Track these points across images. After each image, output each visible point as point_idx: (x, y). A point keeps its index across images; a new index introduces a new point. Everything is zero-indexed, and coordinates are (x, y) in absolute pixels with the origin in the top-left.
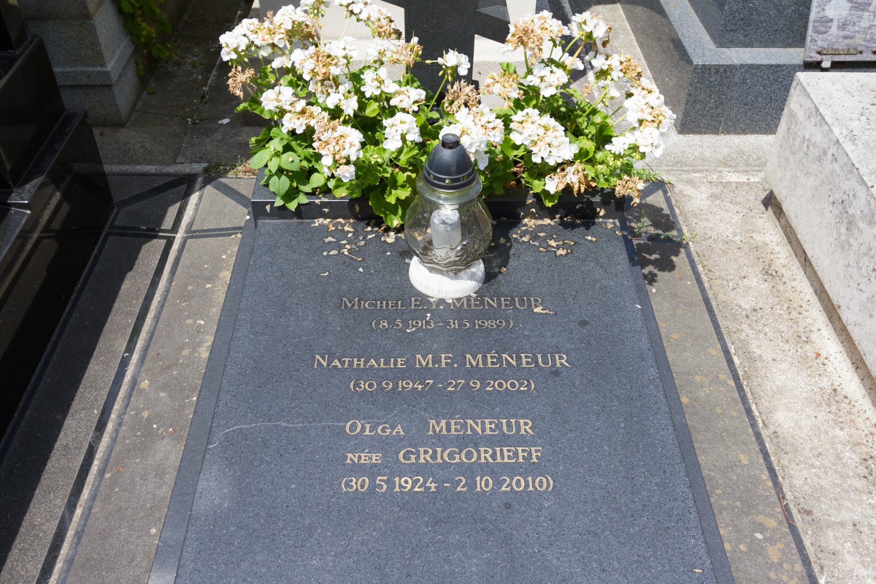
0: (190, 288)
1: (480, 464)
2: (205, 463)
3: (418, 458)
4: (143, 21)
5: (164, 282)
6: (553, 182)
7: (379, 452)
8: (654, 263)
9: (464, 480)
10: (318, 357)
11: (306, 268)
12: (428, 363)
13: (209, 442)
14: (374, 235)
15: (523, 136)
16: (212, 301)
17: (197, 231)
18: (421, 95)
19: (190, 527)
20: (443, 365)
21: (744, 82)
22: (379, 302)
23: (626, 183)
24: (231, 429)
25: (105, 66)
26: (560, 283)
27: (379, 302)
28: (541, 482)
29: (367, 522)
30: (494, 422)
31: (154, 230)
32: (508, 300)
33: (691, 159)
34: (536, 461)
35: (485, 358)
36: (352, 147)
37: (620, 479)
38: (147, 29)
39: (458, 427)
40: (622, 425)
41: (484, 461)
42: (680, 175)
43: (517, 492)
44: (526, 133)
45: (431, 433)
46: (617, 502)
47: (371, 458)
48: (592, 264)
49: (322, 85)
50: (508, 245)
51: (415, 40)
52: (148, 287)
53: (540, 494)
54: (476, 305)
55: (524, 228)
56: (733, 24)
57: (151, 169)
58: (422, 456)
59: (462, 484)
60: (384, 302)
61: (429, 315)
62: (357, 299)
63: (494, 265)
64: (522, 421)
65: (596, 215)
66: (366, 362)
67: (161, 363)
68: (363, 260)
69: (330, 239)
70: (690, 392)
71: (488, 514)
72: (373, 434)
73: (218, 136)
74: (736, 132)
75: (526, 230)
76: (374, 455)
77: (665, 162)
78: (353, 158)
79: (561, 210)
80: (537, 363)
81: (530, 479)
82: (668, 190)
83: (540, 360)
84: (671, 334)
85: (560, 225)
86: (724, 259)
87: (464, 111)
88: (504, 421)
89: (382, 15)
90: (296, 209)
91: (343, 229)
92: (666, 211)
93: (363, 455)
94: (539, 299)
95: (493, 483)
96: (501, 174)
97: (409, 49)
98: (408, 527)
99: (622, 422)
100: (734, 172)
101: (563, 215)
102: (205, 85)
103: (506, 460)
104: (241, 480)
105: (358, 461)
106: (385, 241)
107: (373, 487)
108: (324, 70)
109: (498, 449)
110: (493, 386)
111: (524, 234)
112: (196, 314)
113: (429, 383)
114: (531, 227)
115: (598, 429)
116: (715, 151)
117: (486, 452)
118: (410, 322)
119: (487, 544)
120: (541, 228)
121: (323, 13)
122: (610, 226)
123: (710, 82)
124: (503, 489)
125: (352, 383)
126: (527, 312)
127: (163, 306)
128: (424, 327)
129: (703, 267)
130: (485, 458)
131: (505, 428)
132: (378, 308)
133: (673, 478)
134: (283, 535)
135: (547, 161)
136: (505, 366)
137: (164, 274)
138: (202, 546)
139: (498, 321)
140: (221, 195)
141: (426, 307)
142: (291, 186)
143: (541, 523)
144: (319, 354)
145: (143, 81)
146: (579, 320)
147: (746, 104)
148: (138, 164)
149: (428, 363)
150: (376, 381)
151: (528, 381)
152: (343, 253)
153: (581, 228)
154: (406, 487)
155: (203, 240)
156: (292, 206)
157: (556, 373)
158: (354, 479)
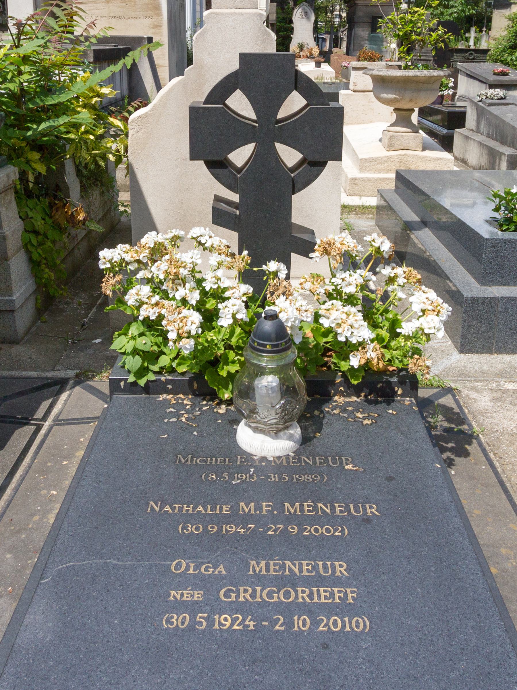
0: (49, 464)
1: (298, 603)
2: (36, 597)
3: (238, 596)
4: (46, 268)
5: (28, 460)
6: (356, 359)
7: (201, 590)
8: (451, 450)
9: (282, 619)
10: (151, 503)
11: (148, 431)
12: (250, 510)
13: (42, 578)
14: (208, 407)
15: (330, 320)
16: (66, 475)
17: (63, 420)
18: (249, 290)
19: (10, 661)
20: (264, 512)
21: (506, 311)
22: (209, 459)
23: (417, 361)
24: (64, 566)
25: (12, 296)
26: (368, 446)
27: (209, 459)
28: (357, 622)
29: (185, 659)
30: (311, 564)
31: (27, 419)
32: (322, 459)
33: (472, 372)
34: (352, 601)
35: (302, 507)
36: (193, 325)
37: (436, 621)
38: (48, 274)
39: (277, 568)
40: (433, 569)
41: (301, 600)
42: (465, 383)
43: (334, 632)
44: (332, 318)
45: (251, 572)
46: (434, 645)
47: (193, 596)
48: (395, 432)
49: (173, 283)
50: (322, 416)
51: (246, 252)
52: (13, 463)
53: (357, 635)
54: (293, 463)
55: (335, 404)
56: (491, 268)
57: (33, 374)
58: (242, 595)
59: (280, 622)
60: (214, 459)
61: (252, 470)
62: (190, 456)
63: (310, 431)
64: (337, 564)
65: (395, 393)
66: (194, 508)
67: (12, 528)
68: (198, 426)
69: (172, 410)
70: (498, 563)
71: (305, 655)
72: (196, 572)
73: (91, 351)
74: (508, 353)
75: (336, 405)
76: (196, 592)
77: (452, 374)
78: (193, 333)
79: (365, 389)
80: (349, 512)
81: (346, 619)
82: (456, 394)
83: (352, 509)
84: (473, 509)
85: (365, 401)
86: (512, 448)
87: (283, 298)
88: (320, 563)
89: (222, 243)
90: (145, 385)
91: (183, 403)
92: (457, 410)
93: (185, 592)
94: (350, 459)
95: (311, 623)
96: (314, 356)
97: (241, 259)
98: (225, 666)
99: (432, 566)
100: (509, 382)
101: (367, 394)
102: (86, 318)
103: (323, 600)
104: (67, 615)
105: (180, 598)
106: (217, 412)
107: (194, 623)
108: (175, 271)
109: (315, 589)
110: (310, 531)
111: (335, 408)
112: (51, 486)
113: (250, 527)
114: (341, 403)
115: (410, 573)
116: (491, 366)
117: (303, 592)
118: (236, 475)
119: (305, 686)
120: (349, 404)
121: (178, 245)
122: (407, 403)
123: (479, 311)
124: (321, 628)
125: (181, 526)
126: (339, 468)
127: (24, 478)
128: (248, 480)
129: (495, 454)
130: (303, 598)
131: (321, 570)
132: (208, 463)
133: (488, 621)
134: (100, 671)
135: (350, 340)
136: (320, 513)
137: (29, 453)
138: (18, 681)
139: (313, 476)
140: (86, 393)
141: (250, 464)
142: (142, 365)
143: (359, 665)
144: (152, 501)
145: (39, 312)
146: (385, 476)
147: (511, 329)
148: (24, 371)
149: (250, 510)
150: (202, 525)
151: (342, 527)
152: (181, 420)
153: (383, 404)
154: (225, 625)
155: (66, 427)
156: (142, 382)
157: (367, 520)
158: (175, 616)
